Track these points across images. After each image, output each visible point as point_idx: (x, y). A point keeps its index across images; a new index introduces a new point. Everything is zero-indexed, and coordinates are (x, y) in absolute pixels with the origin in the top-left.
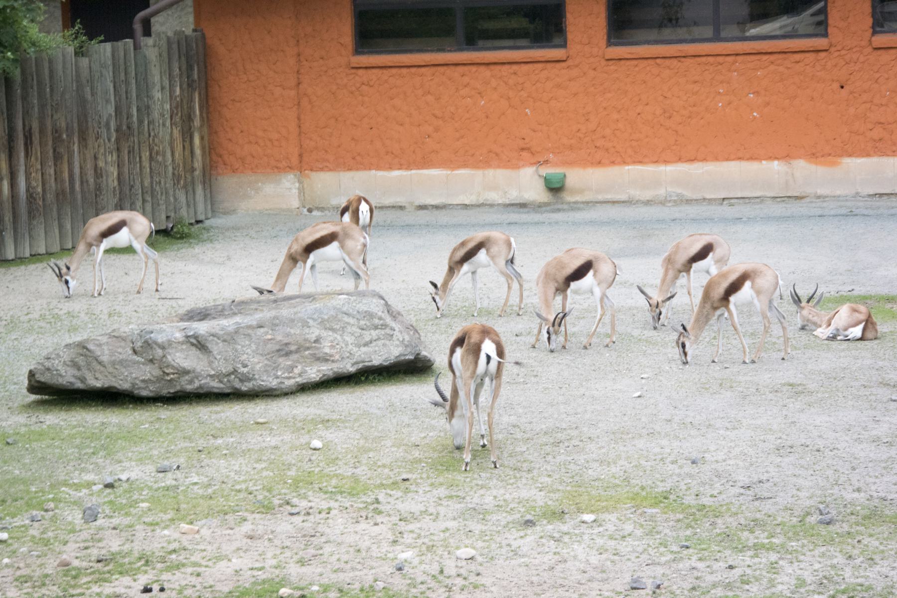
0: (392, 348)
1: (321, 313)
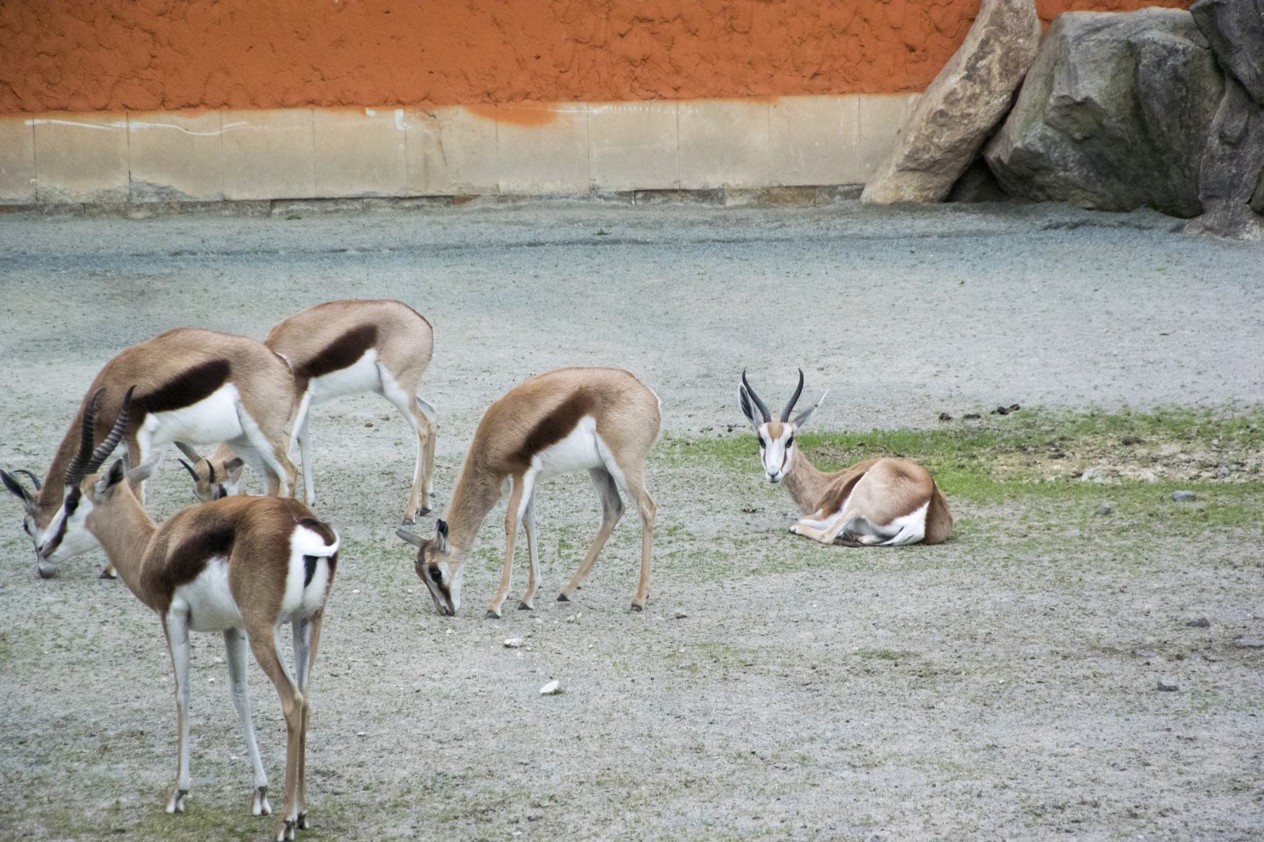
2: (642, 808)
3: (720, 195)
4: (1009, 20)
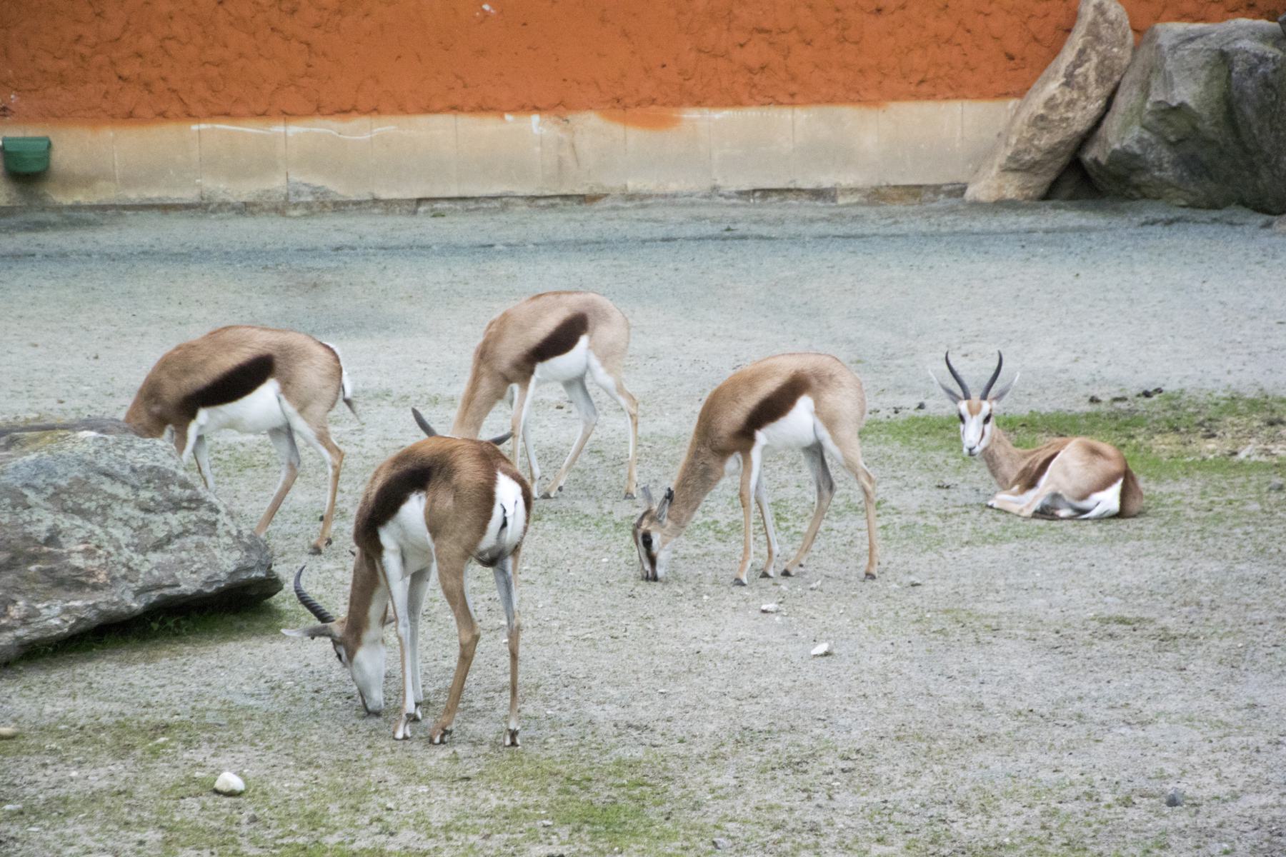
0: (217, 552)
1: (51, 473)
2: (947, 761)
3: (832, 194)
4: (1104, 31)
